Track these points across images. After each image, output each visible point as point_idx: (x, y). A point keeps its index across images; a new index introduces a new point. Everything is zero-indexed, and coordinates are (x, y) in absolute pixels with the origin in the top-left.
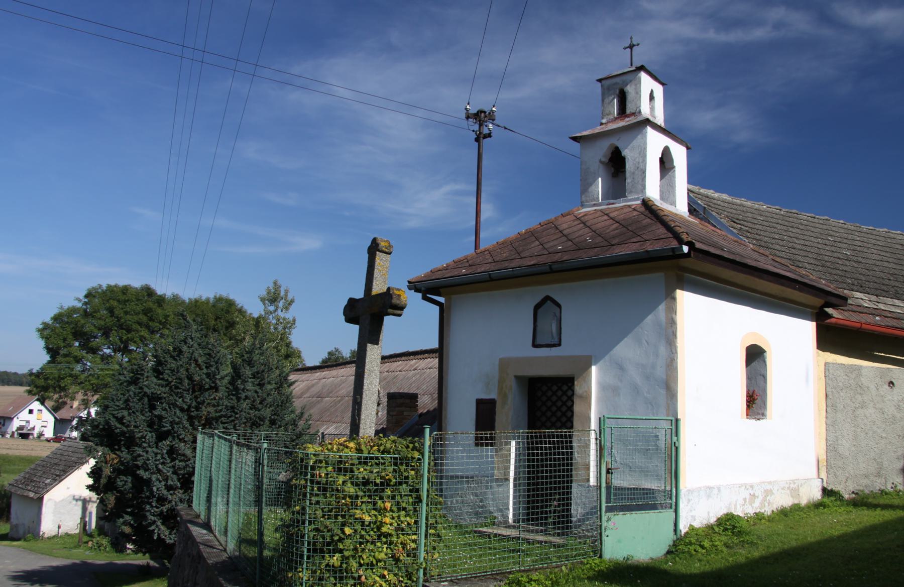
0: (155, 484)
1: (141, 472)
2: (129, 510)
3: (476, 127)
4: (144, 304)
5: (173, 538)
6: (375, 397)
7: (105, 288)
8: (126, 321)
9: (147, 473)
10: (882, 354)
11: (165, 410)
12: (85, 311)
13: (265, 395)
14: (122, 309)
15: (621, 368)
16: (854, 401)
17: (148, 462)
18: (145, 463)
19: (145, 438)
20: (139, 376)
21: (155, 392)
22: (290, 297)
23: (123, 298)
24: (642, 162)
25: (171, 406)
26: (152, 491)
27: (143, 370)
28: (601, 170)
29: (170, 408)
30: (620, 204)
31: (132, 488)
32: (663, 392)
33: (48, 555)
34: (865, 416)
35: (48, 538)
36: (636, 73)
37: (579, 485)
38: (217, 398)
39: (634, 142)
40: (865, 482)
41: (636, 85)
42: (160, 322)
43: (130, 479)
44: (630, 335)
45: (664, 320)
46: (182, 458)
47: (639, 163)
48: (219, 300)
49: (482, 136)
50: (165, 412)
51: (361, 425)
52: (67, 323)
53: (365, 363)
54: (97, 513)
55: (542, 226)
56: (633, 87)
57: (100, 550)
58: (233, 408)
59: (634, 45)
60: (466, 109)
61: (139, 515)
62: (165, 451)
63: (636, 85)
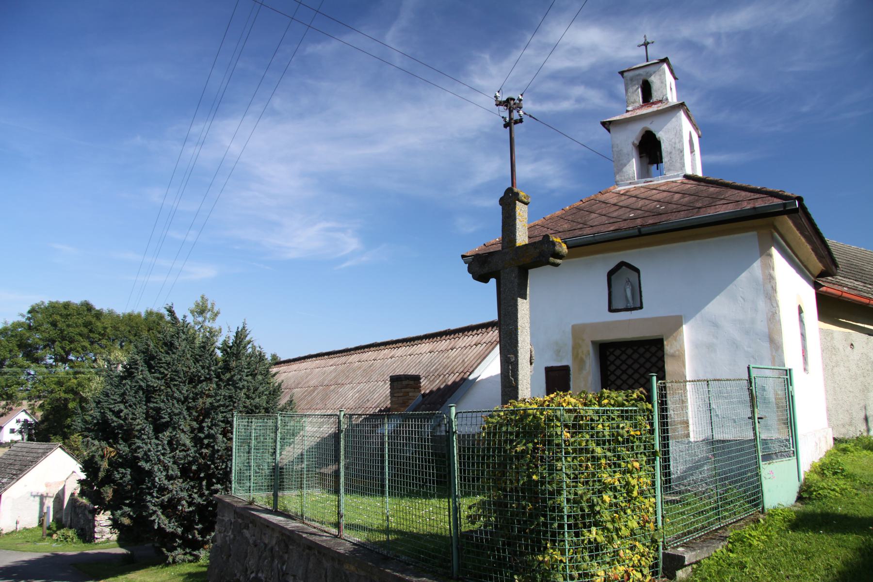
0: (157, 474)
1: (142, 464)
2: (128, 502)
3: (506, 114)
4: (84, 318)
5: (172, 527)
7: (47, 305)
8: (69, 333)
9: (148, 464)
10: (844, 321)
11: (163, 401)
12: (29, 326)
13: (257, 385)
14: (65, 322)
17: (149, 453)
18: (146, 454)
19: (144, 430)
20: (133, 370)
21: (152, 385)
22: (216, 310)
23: (65, 313)
24: (679, 142)
25: (169, 398)
26: (153, 481)
27: (137, 364)
28: (634, 153)
29: (168, 400)
30: (658, 181)
31: (131, 480)
32: (766, 345)
33: (14, 550)
34: (839, 373)
35: (6, 534)
37: (678, 442)
38: (211, 389)
39: (667, 125)
40: (843, 430)
41: (660, 75)
42: (99, 334)
43: (129, 471)
44: (723, 293)
46: (183, 448)
47: (675, 143)
48: (150, 314)
49: (513, 121)
50: (163, 404)
51: (519, 386)
52: (12, 336)
53: (517, 318)
54: (54, 508)
56: (658, 77)
57: (67, 541)
58: (231, 397)
59: (648, 43)
60: (496, 97)
61: (139, 505)
62: (166, 442)
63: (660, 75)
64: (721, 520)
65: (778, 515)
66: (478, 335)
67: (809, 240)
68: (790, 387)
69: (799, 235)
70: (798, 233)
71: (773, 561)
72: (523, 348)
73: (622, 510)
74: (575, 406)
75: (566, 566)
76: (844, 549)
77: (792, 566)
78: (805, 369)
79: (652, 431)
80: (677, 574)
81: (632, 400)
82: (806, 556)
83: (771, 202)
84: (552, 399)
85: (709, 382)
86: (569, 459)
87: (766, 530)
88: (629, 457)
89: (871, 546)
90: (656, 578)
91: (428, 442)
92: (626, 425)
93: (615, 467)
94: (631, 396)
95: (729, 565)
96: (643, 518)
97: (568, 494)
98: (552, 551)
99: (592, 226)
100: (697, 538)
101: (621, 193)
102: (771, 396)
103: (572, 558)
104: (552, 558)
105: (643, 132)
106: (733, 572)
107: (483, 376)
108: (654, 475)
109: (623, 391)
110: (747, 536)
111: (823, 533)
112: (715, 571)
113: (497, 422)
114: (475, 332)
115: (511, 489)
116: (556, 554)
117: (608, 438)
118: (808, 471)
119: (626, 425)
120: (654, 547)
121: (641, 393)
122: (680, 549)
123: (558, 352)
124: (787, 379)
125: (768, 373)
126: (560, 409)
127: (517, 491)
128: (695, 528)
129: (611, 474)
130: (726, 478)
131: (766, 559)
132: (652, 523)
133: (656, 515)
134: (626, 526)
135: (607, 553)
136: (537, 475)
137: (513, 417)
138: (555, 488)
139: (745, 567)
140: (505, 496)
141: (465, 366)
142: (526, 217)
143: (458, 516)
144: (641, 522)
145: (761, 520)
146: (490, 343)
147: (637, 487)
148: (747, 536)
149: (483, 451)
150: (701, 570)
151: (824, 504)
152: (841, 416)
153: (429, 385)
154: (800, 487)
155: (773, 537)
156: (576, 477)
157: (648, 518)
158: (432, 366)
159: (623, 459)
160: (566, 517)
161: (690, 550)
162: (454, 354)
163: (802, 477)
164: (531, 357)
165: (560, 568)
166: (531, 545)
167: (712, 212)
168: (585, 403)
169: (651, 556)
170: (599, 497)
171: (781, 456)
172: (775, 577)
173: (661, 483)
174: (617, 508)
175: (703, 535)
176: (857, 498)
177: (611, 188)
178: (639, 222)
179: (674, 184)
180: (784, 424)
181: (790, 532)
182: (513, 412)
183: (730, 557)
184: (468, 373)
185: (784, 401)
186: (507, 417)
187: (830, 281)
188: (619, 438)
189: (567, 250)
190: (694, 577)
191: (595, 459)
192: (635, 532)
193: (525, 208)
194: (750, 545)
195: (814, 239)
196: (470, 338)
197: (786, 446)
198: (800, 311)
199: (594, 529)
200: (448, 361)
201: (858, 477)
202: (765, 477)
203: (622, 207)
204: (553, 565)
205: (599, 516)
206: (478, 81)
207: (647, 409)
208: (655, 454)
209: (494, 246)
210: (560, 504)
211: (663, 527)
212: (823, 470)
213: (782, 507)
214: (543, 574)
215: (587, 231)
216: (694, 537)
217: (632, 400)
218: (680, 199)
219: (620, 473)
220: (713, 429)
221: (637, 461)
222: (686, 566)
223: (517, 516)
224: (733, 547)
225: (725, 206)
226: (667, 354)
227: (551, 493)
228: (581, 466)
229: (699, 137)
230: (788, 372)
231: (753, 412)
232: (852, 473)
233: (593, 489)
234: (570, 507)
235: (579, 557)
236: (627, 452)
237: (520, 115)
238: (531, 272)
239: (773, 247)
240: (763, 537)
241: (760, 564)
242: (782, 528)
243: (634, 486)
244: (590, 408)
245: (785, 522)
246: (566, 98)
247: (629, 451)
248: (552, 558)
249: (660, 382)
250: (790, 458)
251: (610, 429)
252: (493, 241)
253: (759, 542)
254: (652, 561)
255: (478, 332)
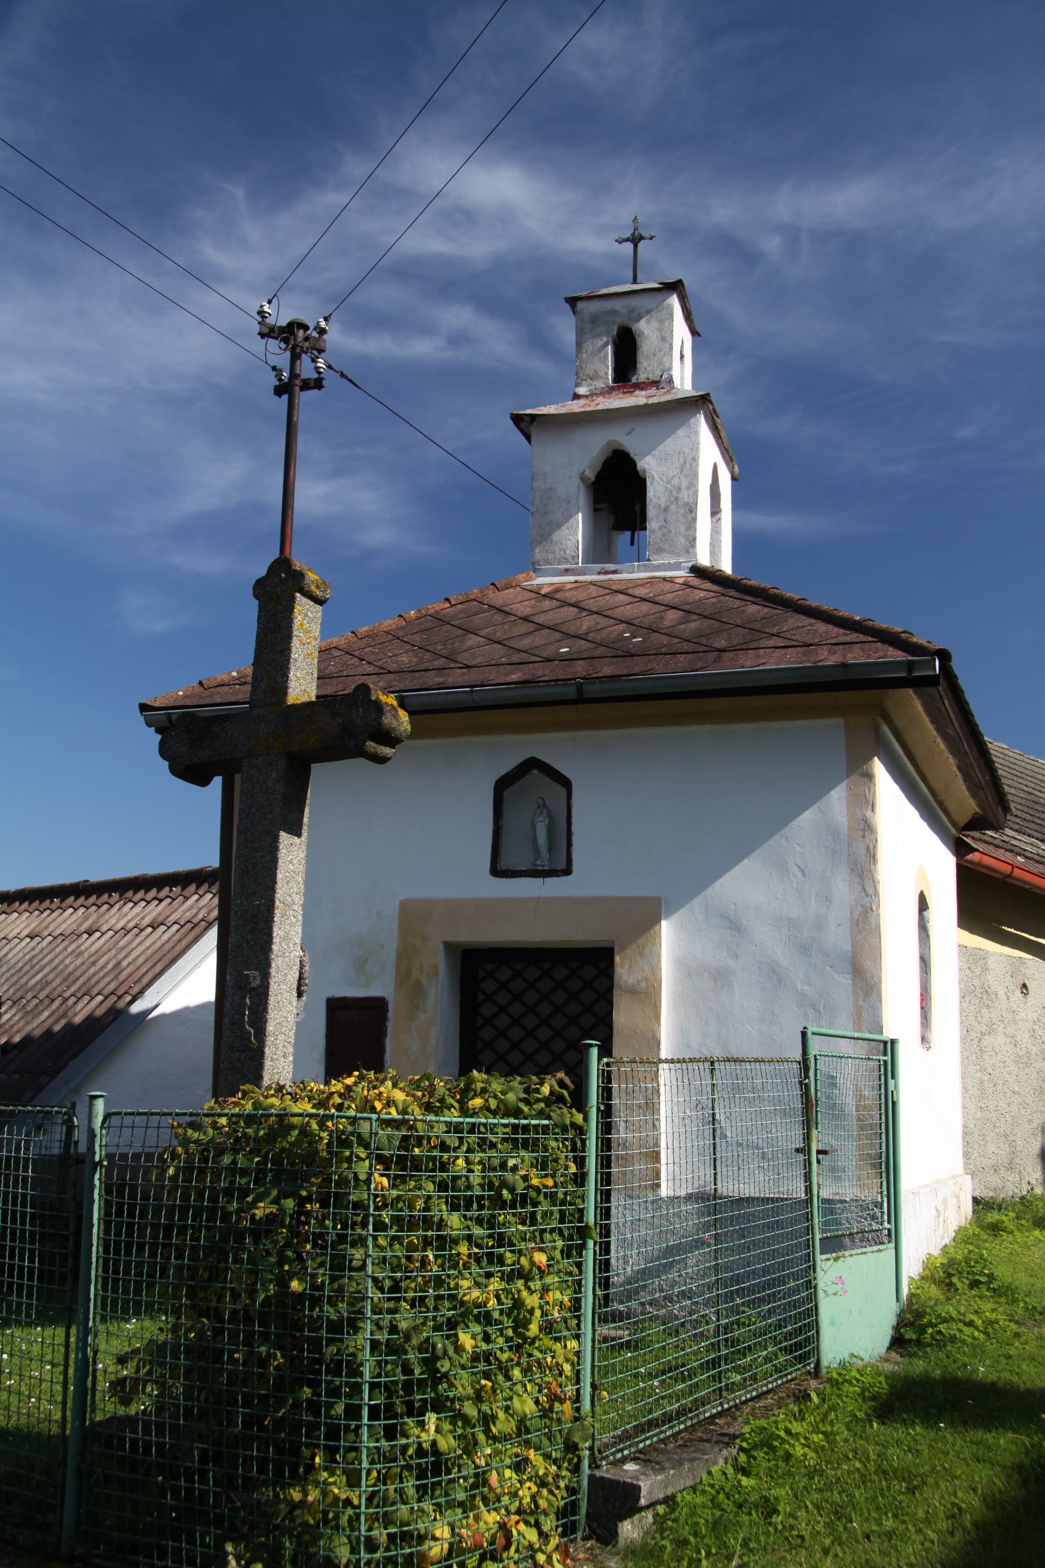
3: (283, 360)
6: (293, 976)
10: (1012, 930)
15: (734, 925)
16: (979, 1019)
24: (688, 488)
28: (583, 499)
30: (632, 573)
32: (845, 981)
36: (658, 297)
40: (994, 1180)
41: (661, 321)
44: (756, 854)
45: (846, 823)
47: (679, 489)
49: (298, 382)
51: (267, 1050)
53: (274, 882)
55: (452, 606)
56: (655, 324)
59: (641, 238)
60: (261, 313)
63: (661, 321)
64: (724, 1393)
65: (851, 1383)
66: (161, 901)
67: (954, 748)
68: (891, 1082)
69: (935, 733)
70: (931, 727)
71: (836, 1497)
72: (283, 956)
73: (500, 1368)
74: (404, 1112)
75: (358, 1516)
76: (988, 1466)
77: (878, 1508)
78: (924, 1039)
79: (580, 1179)
80: (620, 1531)
81: (538, 1100)
82: (909, 1483)
83: (881, 654)
84: (349, 1088)
85: (716, 1064)
86: (382, 1242)
87: (823, 1421)
88: (524, 1239)
89: (1042, 1460)
90: (572, 1541)
91: (24, 1187)
92: (520, 1160)
93: (490, 1262)
94: (537, 1091)
95: (740, 1506)
96: (549, 1389)
97: (374, 1328)
98: (325, 1474)
99: (468, 667)
100: (668, 1438)
101: (543, 592)
102: (848, 1100)
103: (373, 1494)
104: (325, 1493)
105: (608, 453)
106: (747, 1523)
107: (168, 1007)
108: (579, 1283)
109: (519, 1078)
110: (782, 1434)
111: (946, 1428)
112: (707, 1521)
113: (209, 1142)
114: (153, 892)
115: (234, 1313)
116: (334, 1483)
117: (478, 1192)
118: (917, 1278)
119: (523, 1161)
120: (570, 1461)
121: (561, 1084)
122: (630, 1467)
123: (361, 964)
124: (885, 1062)
125: (845, 1047)
126: (370, 1119)
127: (249, 1320)
128: (664, 1414)
129: (479, 1279)
130: (741, 1293)
131: (821, 1490)
132: (568, 1402)
133: (578, 1382)
134: (507, 1409)
135: (459, 1478)
136: (300, 1280)
137: (250, 1131)
138: (345, 1314)
139: (775, 1511)
140: (218, 1332)
141: (122, 977)
142: (317, 634)
143: (89, 1383)
144: (543, 1399)
145: (814, 1395)
146: (190, 926)
147: (538, 1313)
148: (782, 1434)
149: (170, 1215)
150: (675, 1520)
151: (948, 1357)
152: (992, 1148)
153: (22, 1023)
154: (899, 1315)
155: (838, 1438)
156: (396, 1288)
157: (559, 1390)
158: (33, 972)
159: (511, 1244)
160: (366, 1388)
161: (653, 1469)
162: (92, 944)
163: (905, 1291)
164: (300, 978)
165: (344, 1520)
166: (274, 1461)
167: (749, 663)
168: (429, 1103)
169: (562, 1484)
170: (448, 1337)
171: (861, 1241)
172: (840, 1538)
173: (594, 1304)
174: (490, 1364)
175: (681, 1431)
176: (1017, 1344)
177: (521, 577)
178: (580, 669)
179: (668, 586)
180: (873, 1166)
181: (875, 1425)
182: (251, 1119)
183: (741, 1486)
184: (128, 998)
185: (875, 1113)
186: (236, 1131)
187: (989, 839)
188: (505, 1192)
189: (409, 728)
190: (657, 1535)
191: (443, 1243)
192: (528, 1423)
193: (315, 611)
194: (788, 1457)
195: (966, 746)
196: (138, 909)
197: (873, 1217)
198: (923, 905)
199: (431, 1418)
200: (79, 961)
201: (1022, 1294)
202: (825, 1291)
203: (542, 627)
204: (325, 1513)
205: (445, 1385)
206: (212, 253)
207: (573, 1125)
208: (583, 1232)
209: (225, 689)
210: (353, 1355)
211: (593, 1412)
212: (950, 1275)
213: (860, 1363)
214: (299, 1536)
215: (457, 676)
216: (662, 1436)
217: (538, 1100)
218: (679, 623)
219: (502, 1279)
220: (719, 1177)
221: (542, 1250)
222: (641, 1509)
223: (244, 1383)
224: (749, 1462)
225: (778, 653)
226: (620, 987)
227: (335, 1327)
228: (409, 1259)
229: (733, 479)
230: (890, 1047)
231: (807, 1138)
232: (1011, 1284)
233: (434, 1319)
234: (379, 1362)
235: (392, 1492)
236: (520, 1227)
237: (317, 368)
238: (319, 772)
239: (876, 758)
240: (817, 1438)
241: (808, 1504)
242: (858, 1414)
243: (531, 1312)
244: (442, 1119)
245: (864, 1399)
246: (427, 329)
247: (523, 1223)
248: (325, 1493)
249: (605, 1060)
250: (881, 1247)
251: (483, 1171)
252: (222, 677)
253: (807, 1450)
254: (563, 1498)
255: (162, 895)
